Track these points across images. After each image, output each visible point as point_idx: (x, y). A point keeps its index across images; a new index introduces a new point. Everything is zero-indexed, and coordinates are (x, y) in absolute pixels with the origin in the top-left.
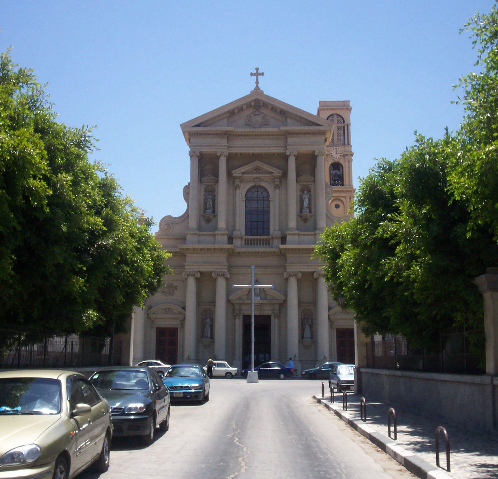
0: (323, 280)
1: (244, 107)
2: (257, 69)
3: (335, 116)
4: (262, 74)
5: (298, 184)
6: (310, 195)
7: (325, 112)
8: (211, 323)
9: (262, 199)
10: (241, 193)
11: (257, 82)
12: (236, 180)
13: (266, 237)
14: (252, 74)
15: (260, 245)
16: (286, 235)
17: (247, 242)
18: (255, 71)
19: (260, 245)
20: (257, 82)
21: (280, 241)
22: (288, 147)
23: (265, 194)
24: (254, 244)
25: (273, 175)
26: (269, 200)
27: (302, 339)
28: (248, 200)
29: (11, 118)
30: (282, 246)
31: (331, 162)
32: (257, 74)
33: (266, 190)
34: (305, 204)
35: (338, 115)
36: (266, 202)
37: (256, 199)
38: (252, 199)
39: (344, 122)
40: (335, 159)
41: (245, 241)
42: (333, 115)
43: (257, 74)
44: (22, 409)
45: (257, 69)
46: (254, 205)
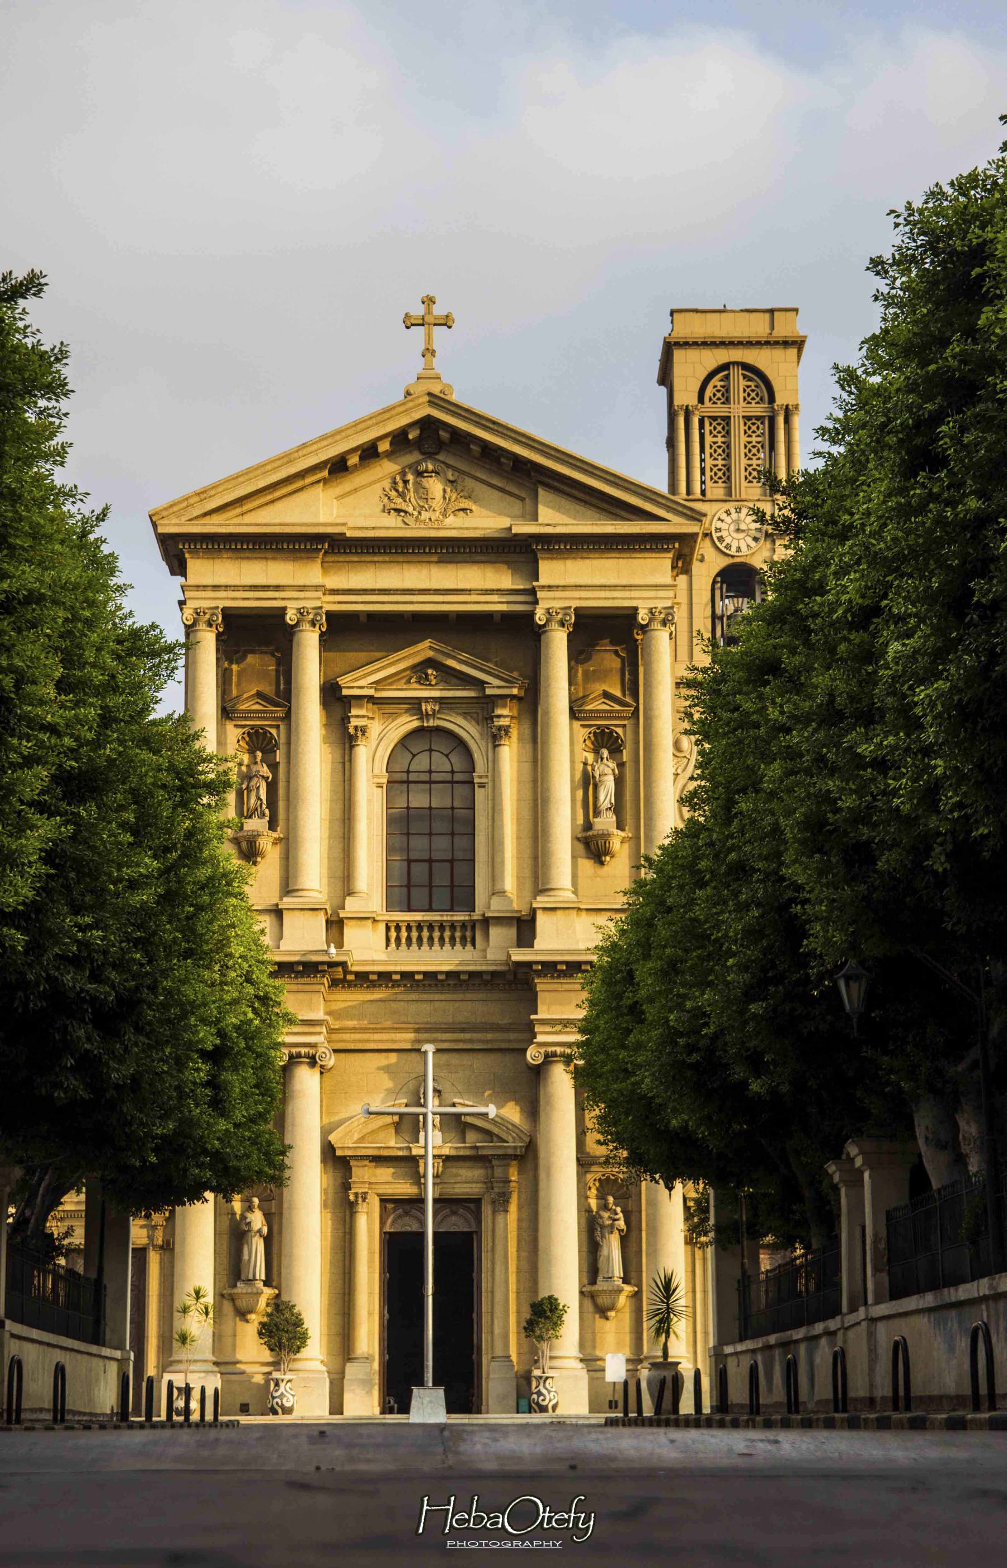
0: (743, 1200)
1: (384, 446)
2: (429, 301)
3: (737, 376)
4: (446, 322)
5: (577, 724)
6: (621, 765)
8: (265, 1230)
9: (448, 777)
10: (371, 759)
11: (429, 352)
12: (354, 712)
13: (460, 917)
15: (453, 944)
17: (393, 934)
18: (418, 310)
19: (453, 944)
20: (429, 352)
21: (512, 932)
23: (457, 761)
24: (453, 939)
26: (472, 783)
27: (593, 1282)
28: (398, 782)
29: (677, 973)
30: (519, 955)
32: (428, 320)
33: (461, 744)
34: (602, 797)
35: (746, 366)
36: (460, 790)
37: (425, 777)
38: (413, 777)
39: (772, 399)
40: (733, 551)
42: (725, 367)
43: (428, 320)
46: (419, 800)
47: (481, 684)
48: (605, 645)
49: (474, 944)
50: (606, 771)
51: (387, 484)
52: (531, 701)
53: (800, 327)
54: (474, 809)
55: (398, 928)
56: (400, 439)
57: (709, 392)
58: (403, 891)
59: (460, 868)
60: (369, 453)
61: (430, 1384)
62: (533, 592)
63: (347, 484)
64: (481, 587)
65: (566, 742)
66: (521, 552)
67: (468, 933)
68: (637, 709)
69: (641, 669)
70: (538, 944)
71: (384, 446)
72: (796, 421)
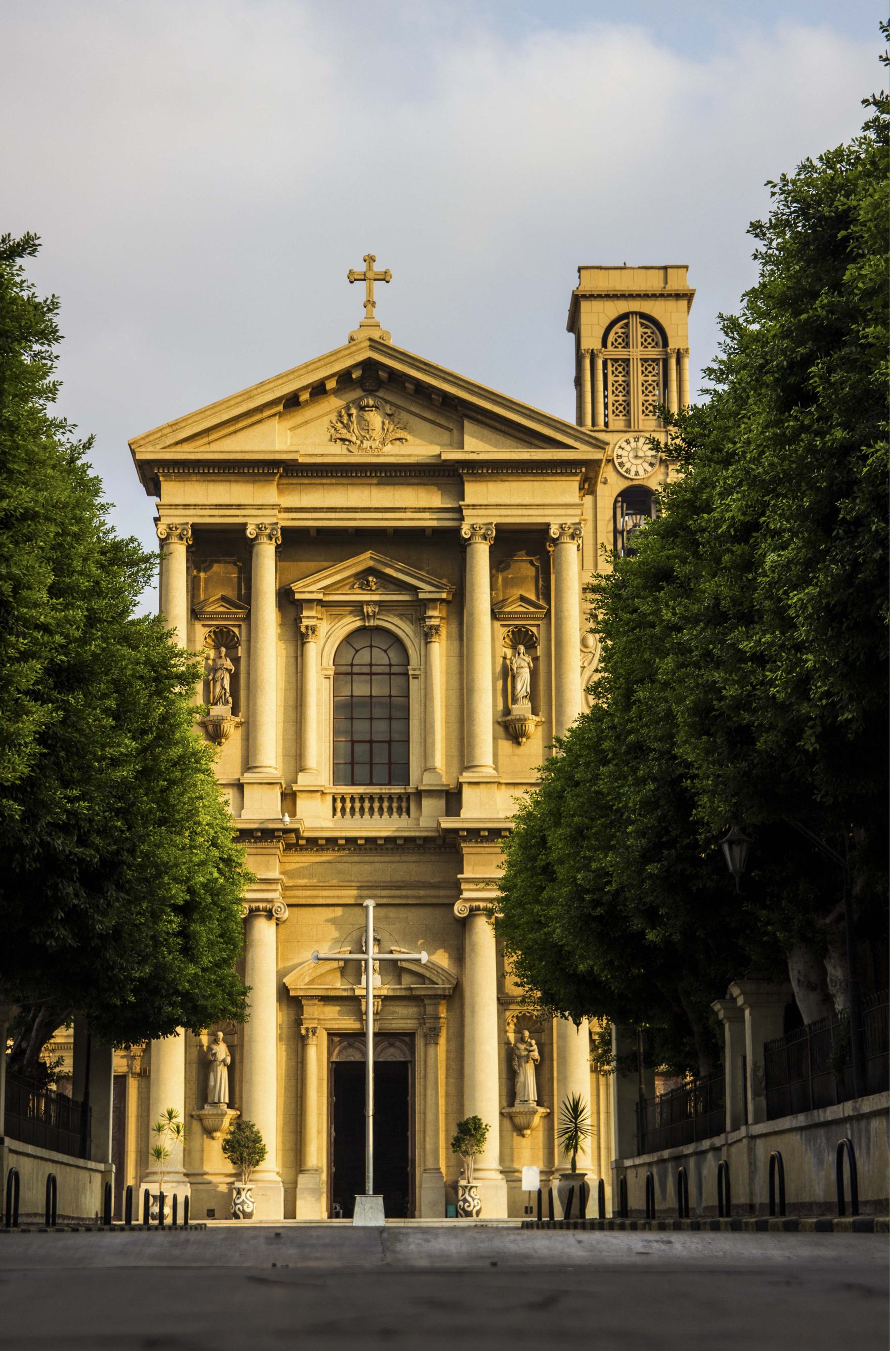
0: (641, 1034)
1: (331, 385)
2: (370, 259)
3: (635, 322)
4: (385, 278)
5: (497, 624)
6: (535, 659)
7: (597, 305)
8: (229, 1060)
9: (386, 670)
10: (320, 654)
11: (370, 303)
12: (305, 613)
13: (397, 790)
14: (353, 278)
16: (460, 785)
17: (339, 805)
18: (360, 267)
20: (370, 303)
21: (441, 803)
22: (465, 512)
23: (394, 656)
25: (421, 596)
27: (511, 1104)
28: (343, 673)
30: (448, 823)
31: (623, 485)
32: (370, 275)
33: (397, 641)
35: (643, 316)
36: (397, 681)
37: (366, 670)
38: (356, 669)
39: (666, 344)
41: (334, 800)
42: (626, 316)
43: (370, 275)
44: (58, 1088)
45: (370, 259)
46: (361, 689)
47: (415, 589)
48: (522, 556)
49: (408, 814)
50: (523, 665)
51: (334, 417)
52: (458, 603)
53: (690, 282)
54: (408, 697)
55: (343, 800)
56: (344, 379)
57: (611, 337)
58: (348, 767)
59: (397, 748)
60: (318, 390)
61: (371, 1193)
62: (459, 510)
63: (299, 417)
64: (415, 506)
65: (488, 640)
66: (449, 475)
67: (404, 804)
68: (549, 611)
69: (553, 577)
70: (465, 813)
71: (331, 385)
72: (687, 363)
